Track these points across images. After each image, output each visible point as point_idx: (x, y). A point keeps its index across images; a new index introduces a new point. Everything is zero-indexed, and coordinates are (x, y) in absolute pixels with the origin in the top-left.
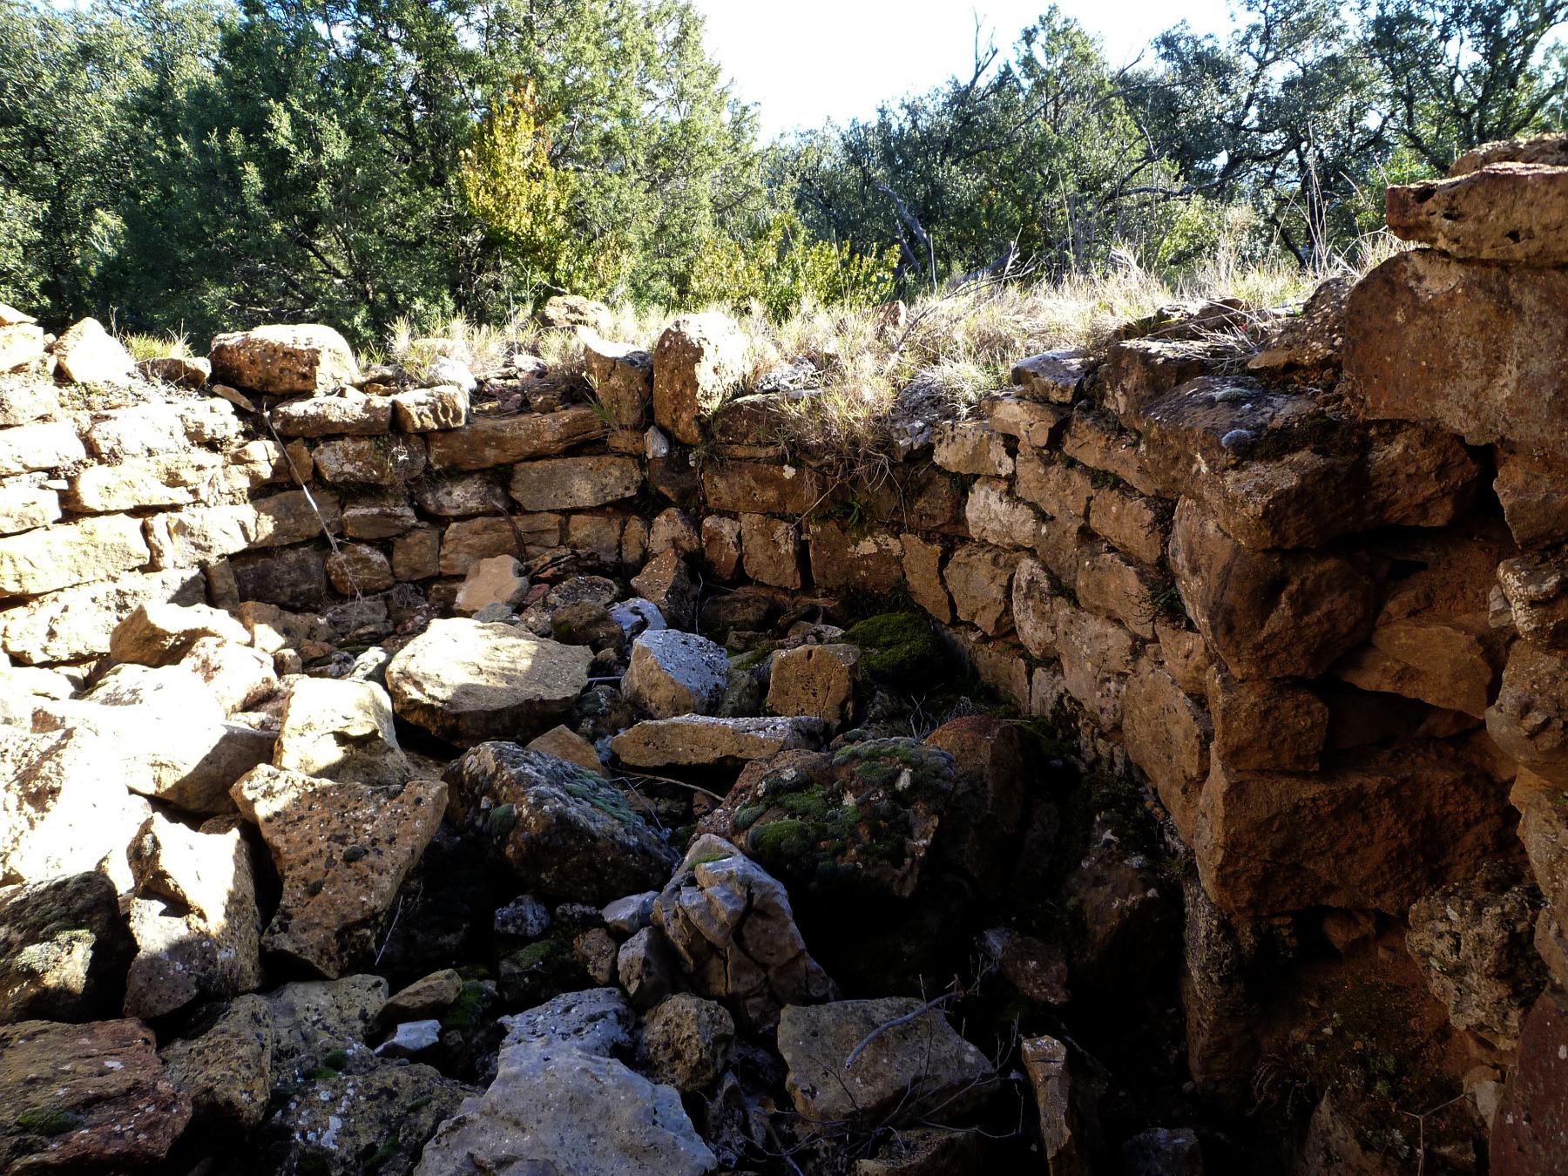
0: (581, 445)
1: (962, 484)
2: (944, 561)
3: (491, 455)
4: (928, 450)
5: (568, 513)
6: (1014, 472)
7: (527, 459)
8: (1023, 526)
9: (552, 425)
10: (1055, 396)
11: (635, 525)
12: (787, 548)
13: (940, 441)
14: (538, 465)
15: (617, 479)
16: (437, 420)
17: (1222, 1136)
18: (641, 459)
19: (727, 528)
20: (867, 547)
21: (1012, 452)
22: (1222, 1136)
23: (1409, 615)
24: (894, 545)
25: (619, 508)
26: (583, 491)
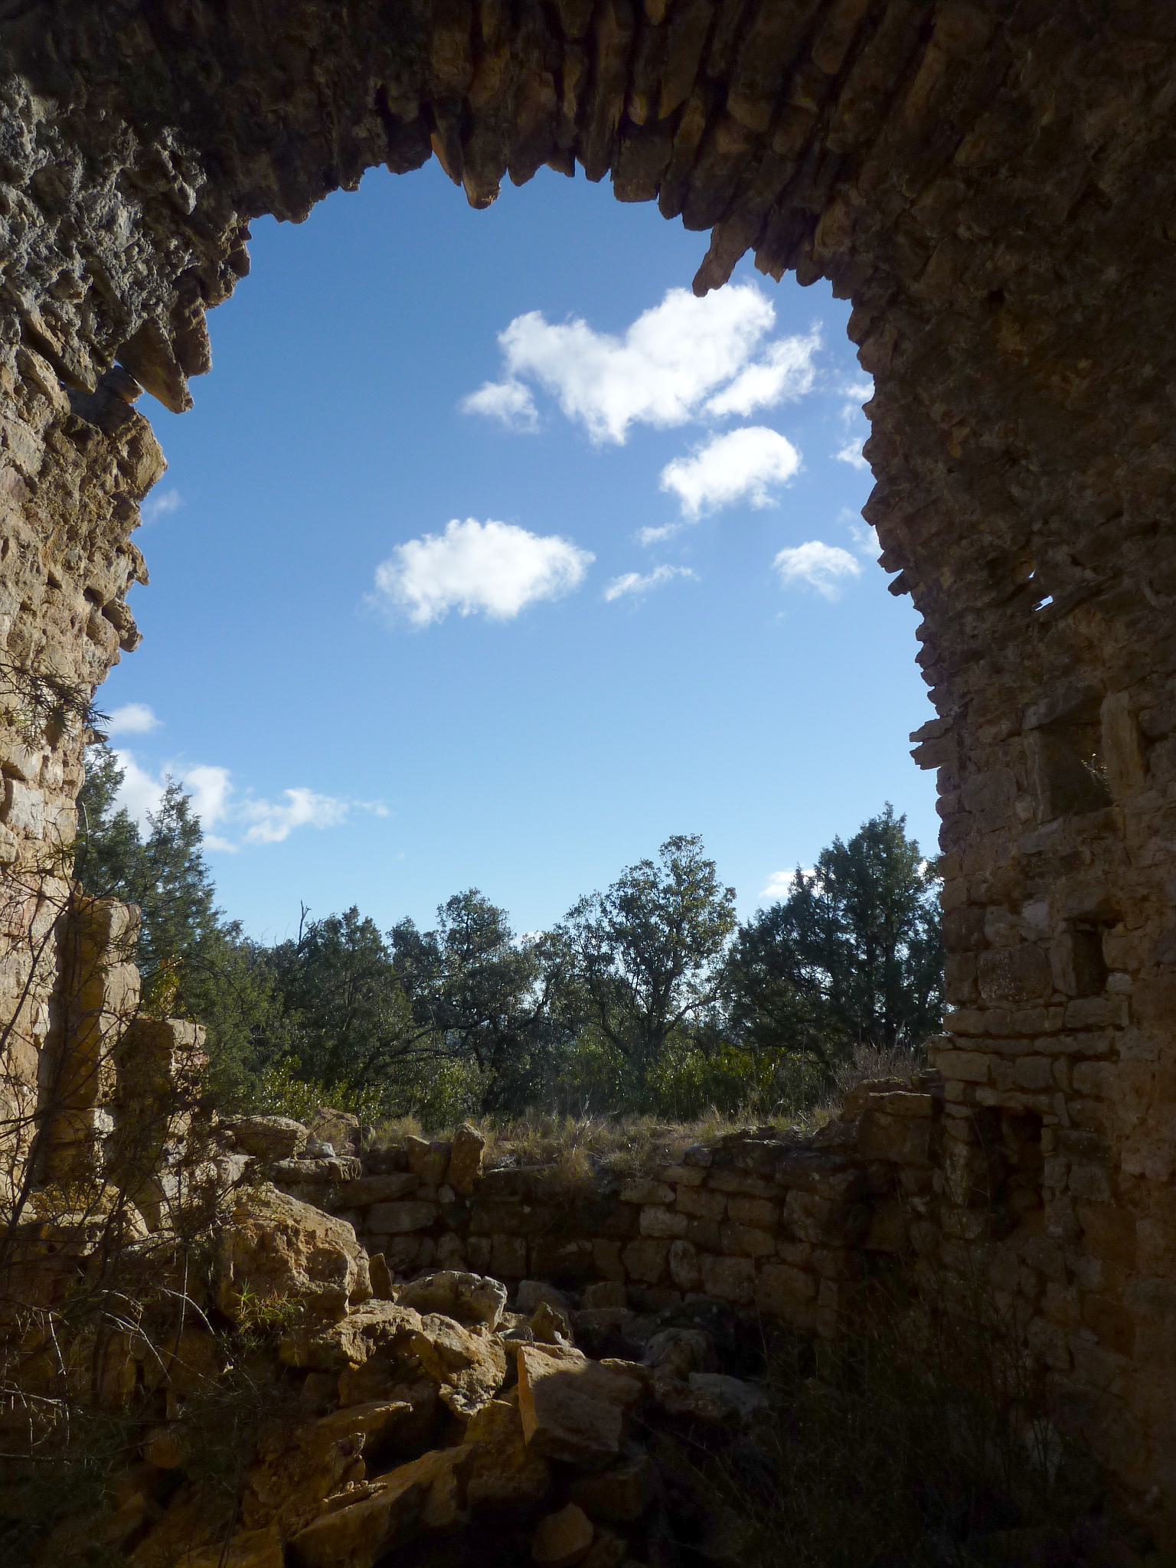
0: (407, 1195)
1: (637, 1208)
2: (621, 1250)
3: (365, 1198)
4: (616, 1193)
5: (393, 1235)
6: (675, 1200)
7: (382, 1201)
8: (680, 1223)
9: (396, 1182)
10: (703, 1163)
11: (429, 1243)
12: (522, 1252)
13: (625, 1189)
14: (383, 1205)
15: (425, 1215)
16: (350, 1174)
17: (1048, 601)
18: (437, 1203)
19: (485, 1243)
20: (572, 1247)
21: (674, 1190)
22: (1048, 601)
23: (1121, 772)
24: (588, 1246)
25: (422, 1233)
26: (406, 1222)
